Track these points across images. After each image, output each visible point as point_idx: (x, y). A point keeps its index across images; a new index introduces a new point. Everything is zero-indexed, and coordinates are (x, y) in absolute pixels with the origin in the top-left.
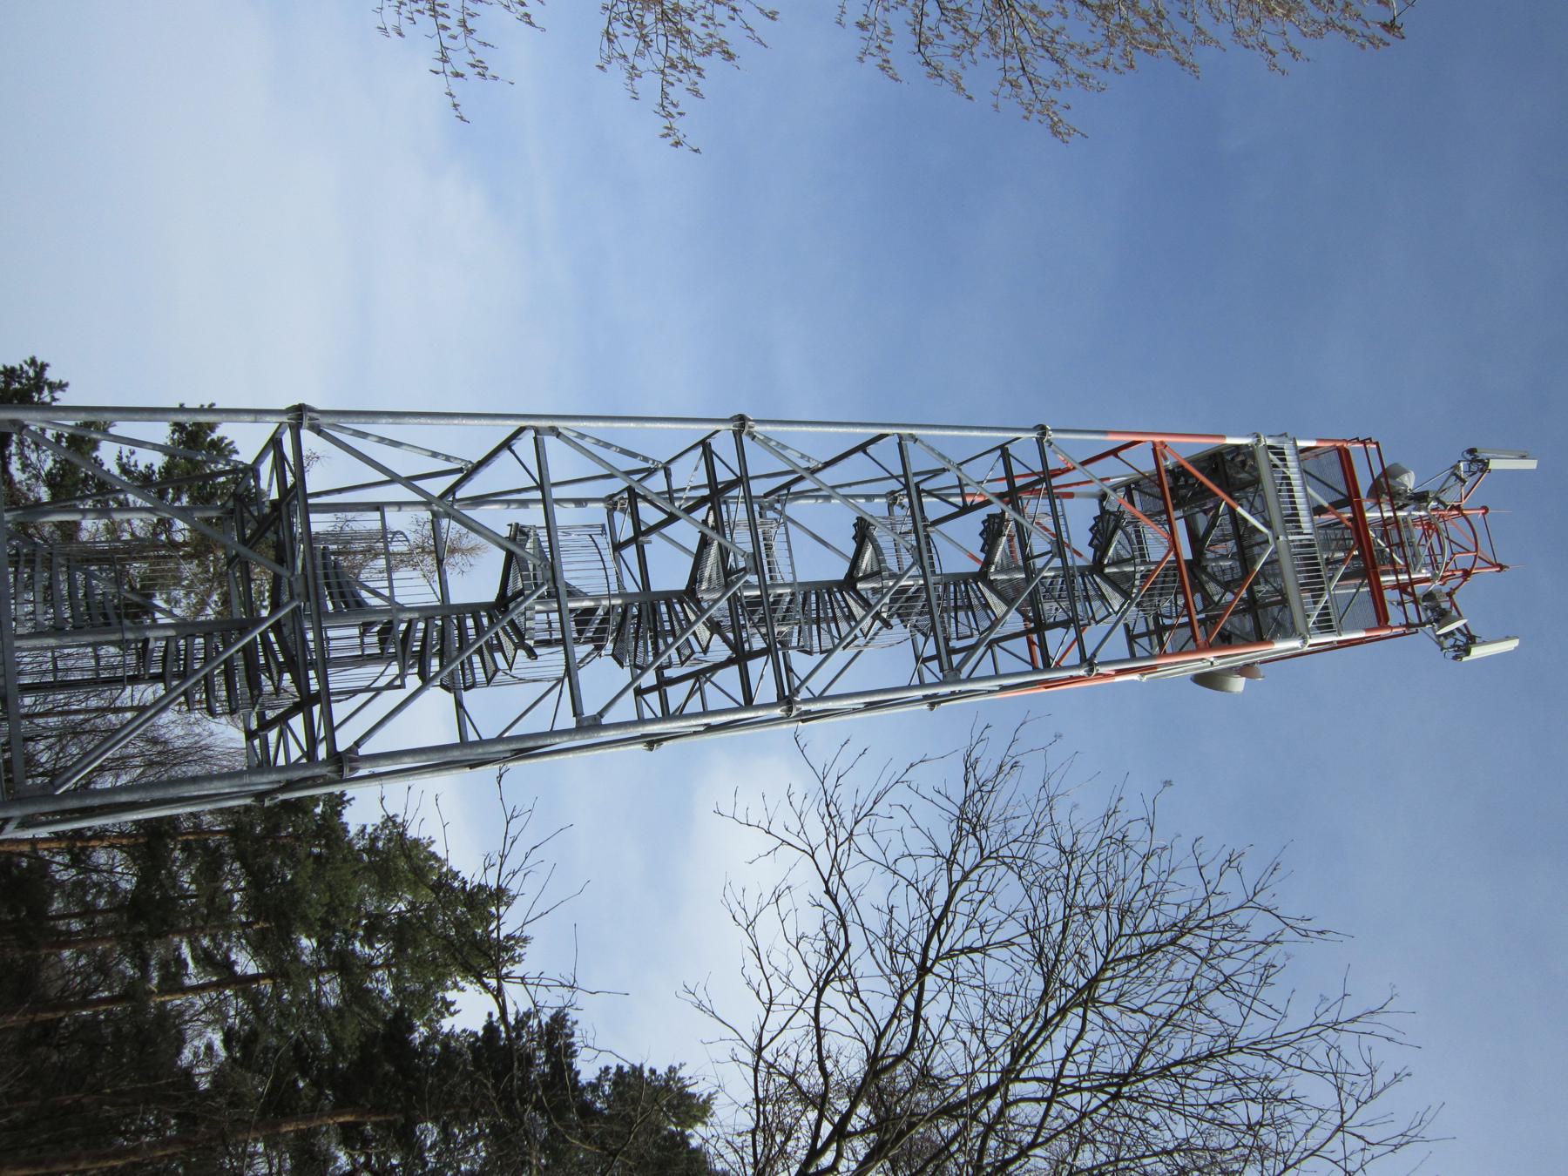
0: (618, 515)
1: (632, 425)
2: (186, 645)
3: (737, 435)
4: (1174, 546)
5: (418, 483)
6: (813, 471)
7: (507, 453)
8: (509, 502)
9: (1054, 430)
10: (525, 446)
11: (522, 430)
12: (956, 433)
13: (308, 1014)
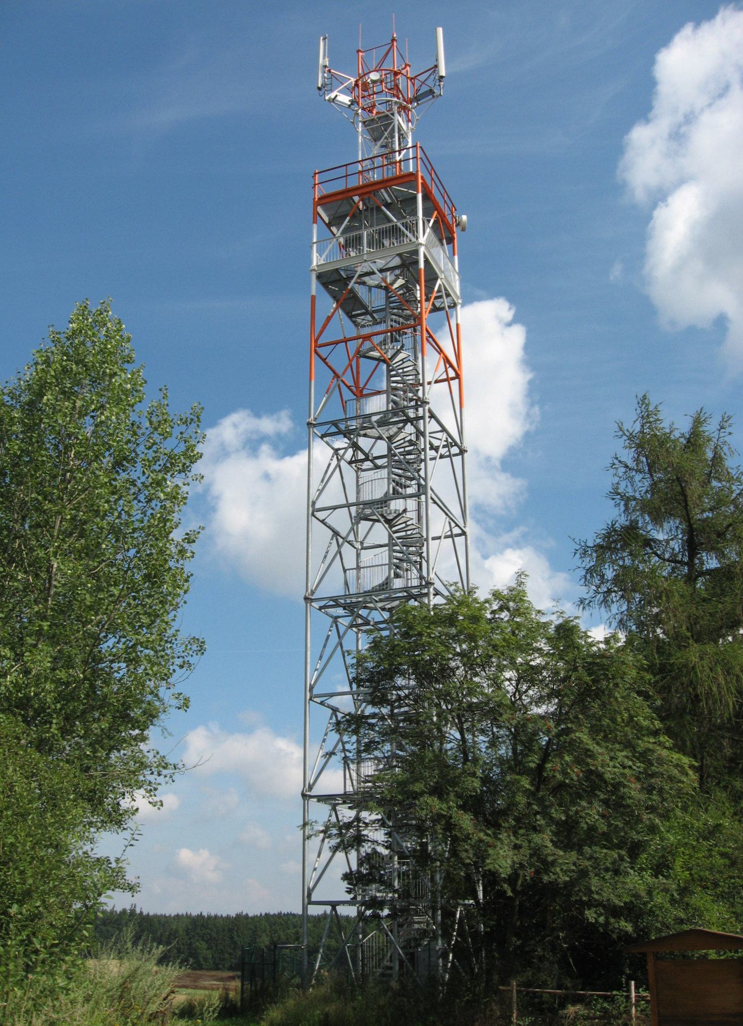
0: (364, 467)
1: (310, 565)
2: (411, 825)
3: (315, 426)
4: (365, 707)
5: (338, 469)
6: (337, 376)
7: (327, 360)
8: (358, 373)
9: (310, 417)
10: (323, 352)
11: (316, 352)
12: (309, 624)
13: (129, 502)
